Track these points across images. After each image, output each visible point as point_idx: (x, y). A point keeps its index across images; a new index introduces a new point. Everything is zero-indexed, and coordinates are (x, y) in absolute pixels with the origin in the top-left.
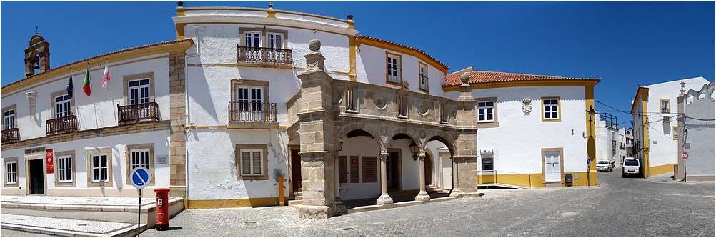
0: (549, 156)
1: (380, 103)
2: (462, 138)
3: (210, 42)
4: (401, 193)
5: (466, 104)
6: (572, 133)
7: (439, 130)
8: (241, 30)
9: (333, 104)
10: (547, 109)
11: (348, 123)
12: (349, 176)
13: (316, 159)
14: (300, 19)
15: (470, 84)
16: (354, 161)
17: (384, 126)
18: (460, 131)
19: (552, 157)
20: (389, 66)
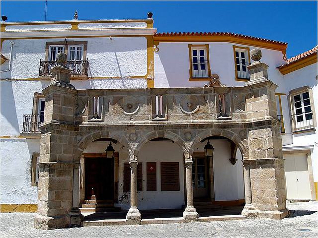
1: (130, 108)
3: (21, 57)
4: (209, 205)
8: (48, 44)
9: (76, 115)
11: (89, 133)
12: (145, 184)
14: (100, 26)
16: (152, 168)
17: (134, 131)
18: (250, 126)
20: (237, 61)
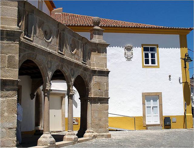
0: (149, 100)
2: (96, 79)
5: (99, 47)
6: (170, 79)
7: (81, 70)
10: (146, 56)
13: (7, 87)
15: (101, 27)
19: (152, 101)
